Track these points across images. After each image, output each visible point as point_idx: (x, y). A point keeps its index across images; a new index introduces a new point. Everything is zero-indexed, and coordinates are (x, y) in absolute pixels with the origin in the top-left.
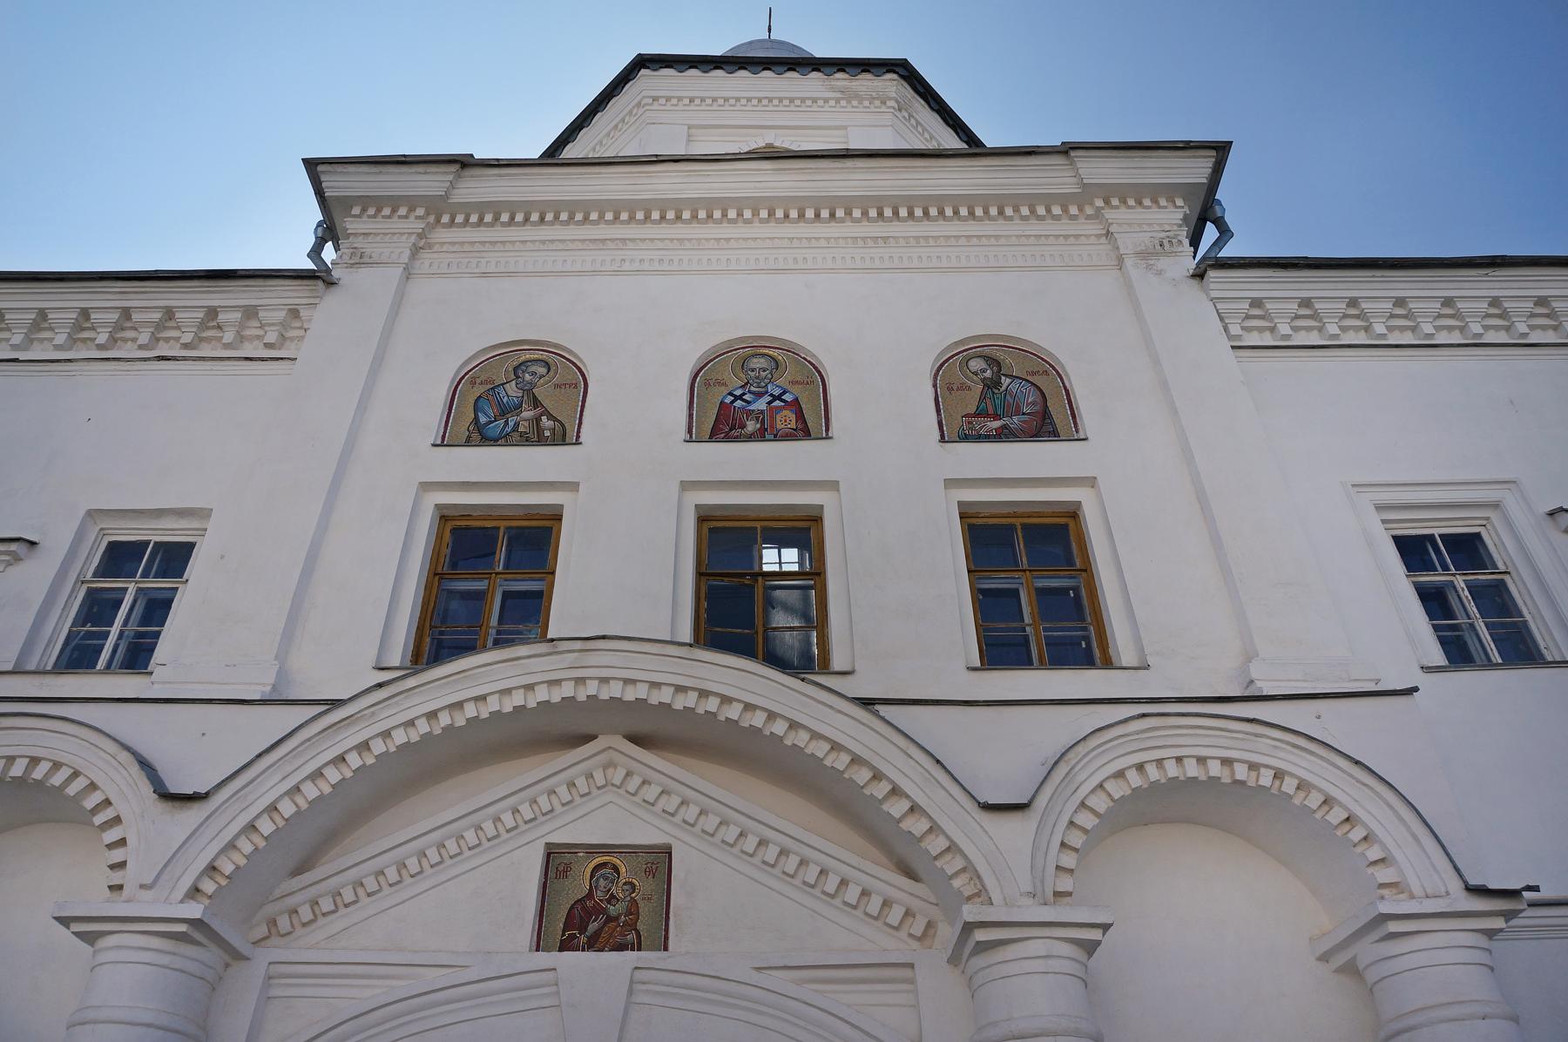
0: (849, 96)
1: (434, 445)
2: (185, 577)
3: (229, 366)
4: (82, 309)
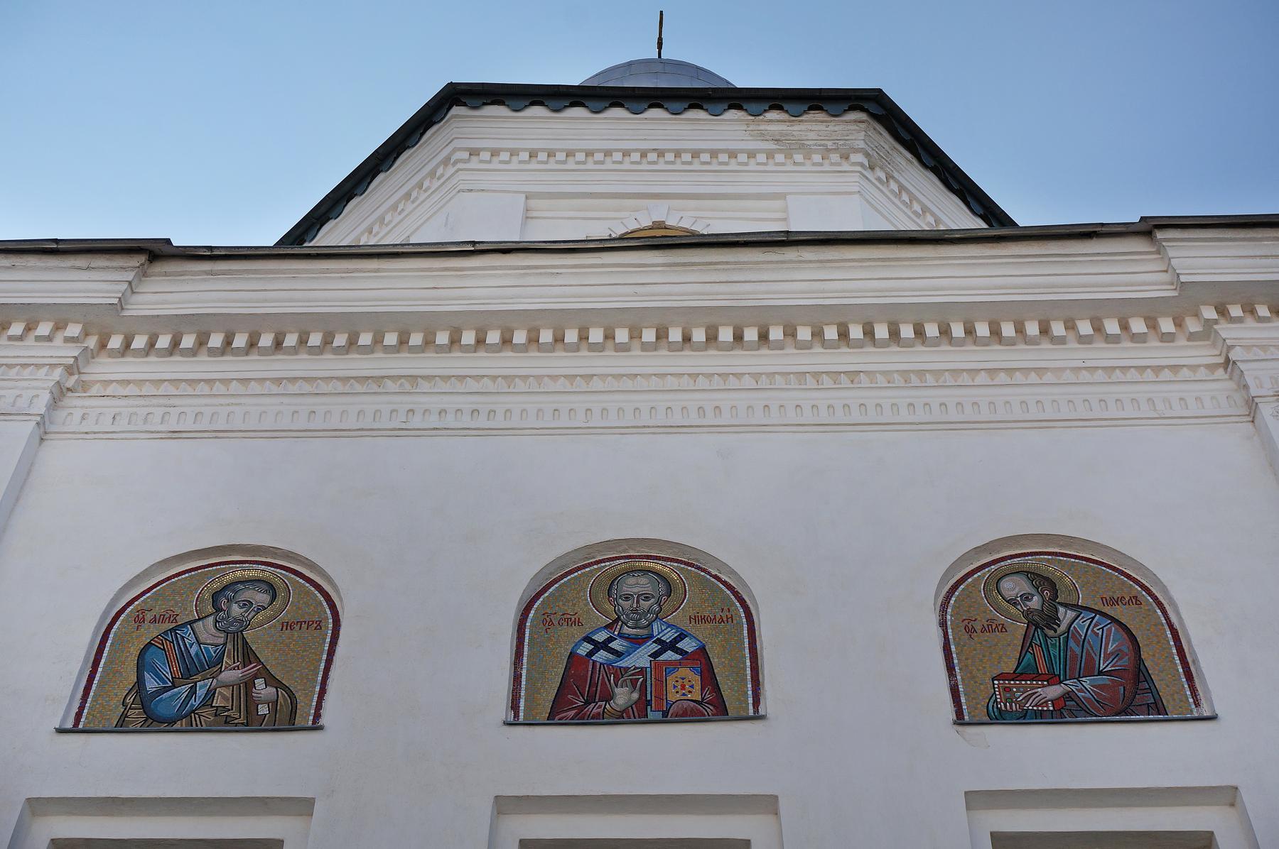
0: (790, 147)
1: (61, 731)
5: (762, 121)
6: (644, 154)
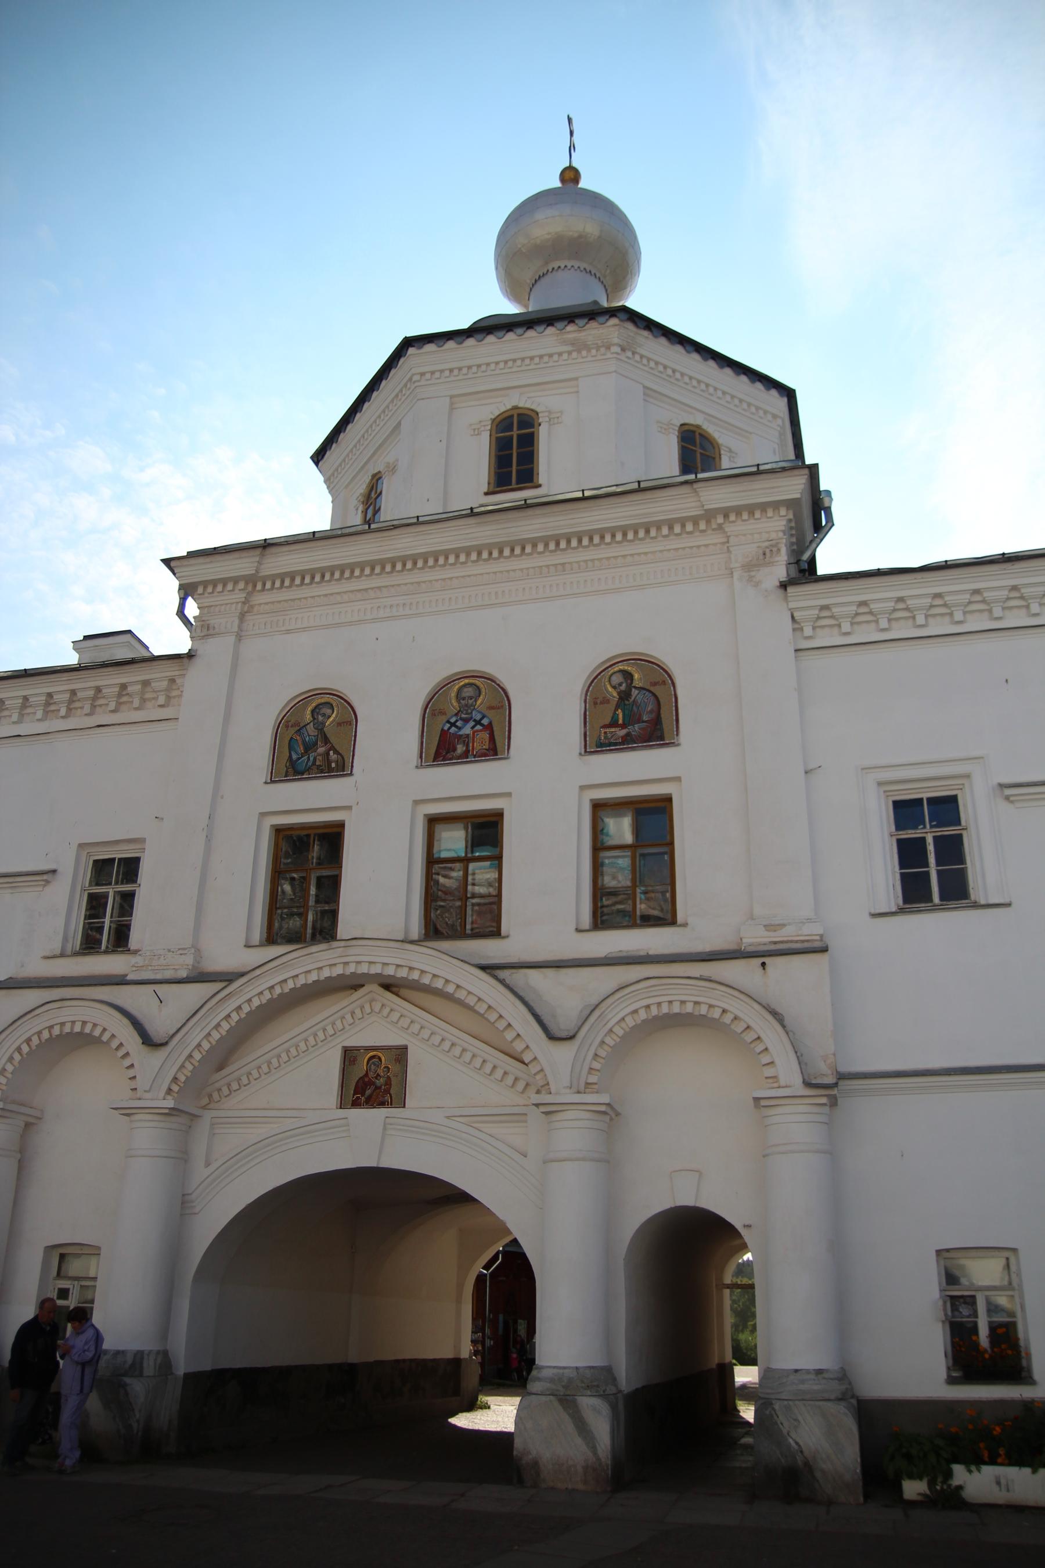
0: (580, 347)
1: (266, 783)
2: (138, 882)
3: (139, 727)
4: (48, 693)
5: (565, 332)
6: (506, 362)
